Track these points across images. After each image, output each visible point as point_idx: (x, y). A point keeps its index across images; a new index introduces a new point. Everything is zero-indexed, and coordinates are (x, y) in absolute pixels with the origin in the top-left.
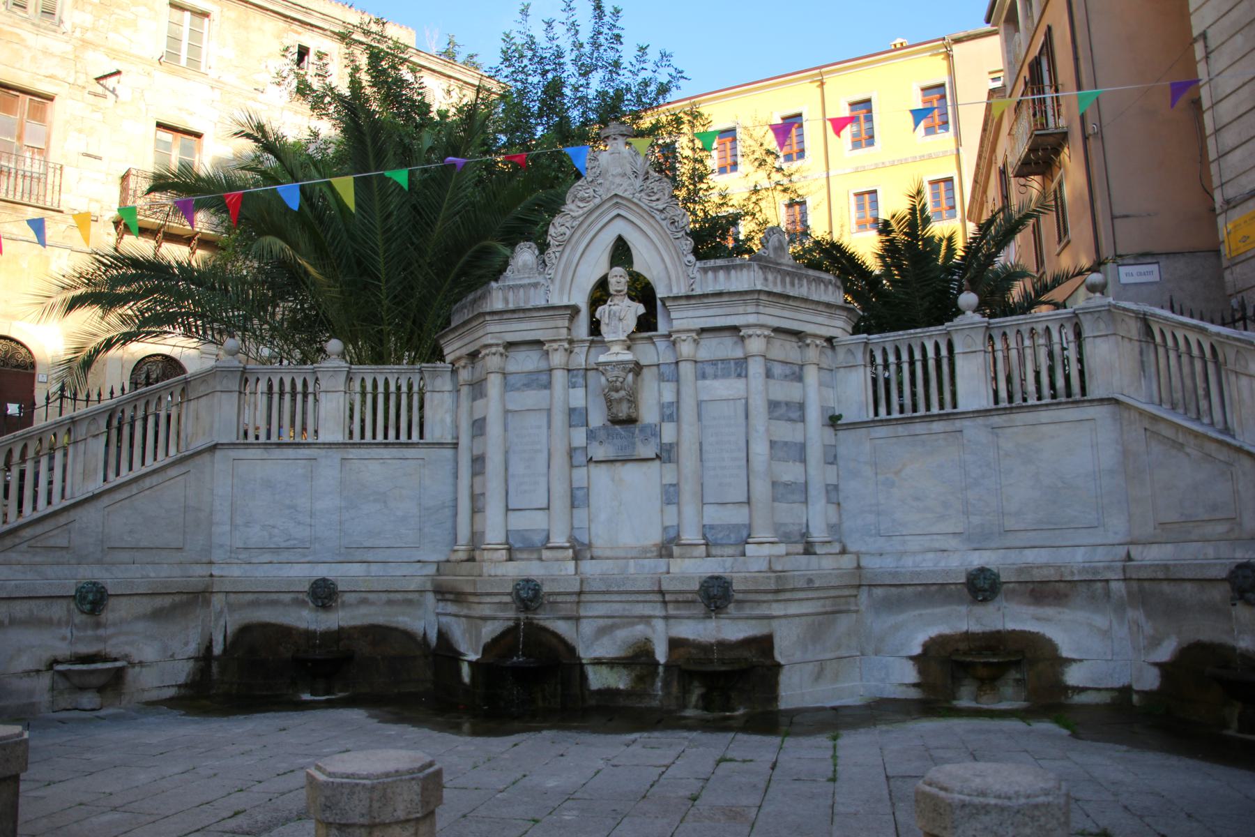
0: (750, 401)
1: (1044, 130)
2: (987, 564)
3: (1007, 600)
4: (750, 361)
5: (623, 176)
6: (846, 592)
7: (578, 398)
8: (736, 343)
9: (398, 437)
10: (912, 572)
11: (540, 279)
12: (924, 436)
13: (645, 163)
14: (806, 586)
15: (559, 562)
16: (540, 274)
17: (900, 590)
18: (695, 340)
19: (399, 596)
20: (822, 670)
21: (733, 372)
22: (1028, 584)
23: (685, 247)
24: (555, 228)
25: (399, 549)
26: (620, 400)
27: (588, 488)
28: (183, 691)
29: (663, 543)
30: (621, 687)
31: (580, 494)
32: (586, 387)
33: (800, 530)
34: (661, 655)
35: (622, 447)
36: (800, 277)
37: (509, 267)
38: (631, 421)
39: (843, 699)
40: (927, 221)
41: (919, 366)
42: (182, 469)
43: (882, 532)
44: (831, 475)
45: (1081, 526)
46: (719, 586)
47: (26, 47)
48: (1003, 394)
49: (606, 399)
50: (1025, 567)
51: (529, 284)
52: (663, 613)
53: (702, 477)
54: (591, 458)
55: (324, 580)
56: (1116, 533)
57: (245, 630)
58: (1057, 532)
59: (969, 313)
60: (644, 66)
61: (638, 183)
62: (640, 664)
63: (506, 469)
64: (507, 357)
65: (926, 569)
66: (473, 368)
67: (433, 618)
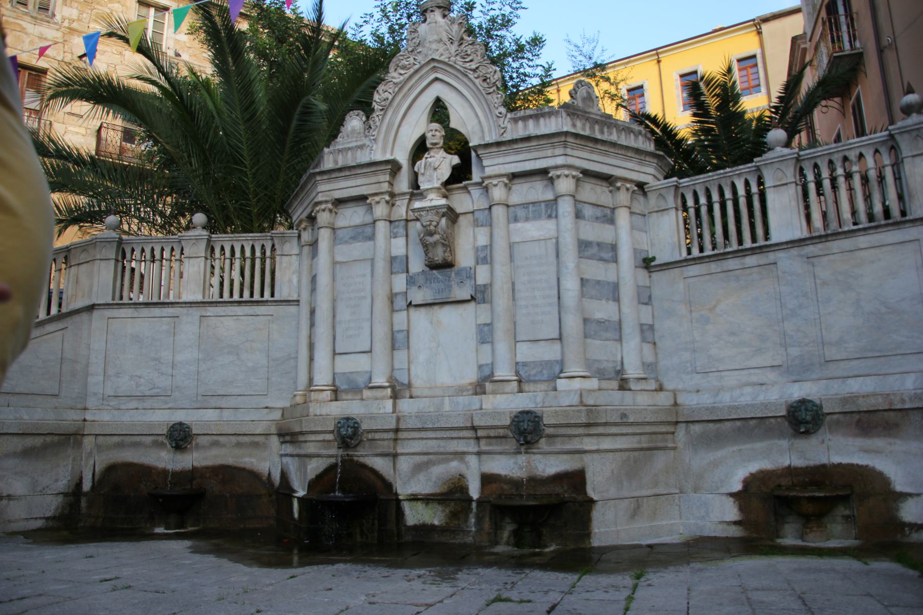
0: (561, 240)
1: (842, 51)
2: (808, 396)
3: (831, 432)
4: (560, 201)
5: (439, 42)
6: (663, 429)
7: (399, 247)
8: (546, 186)
9: (252, 295)
10: (729, 407)
11: (366, 141)
12: (737, 272)
13: (460, 31)
14: (620, 421)
15: (378, 401)
16: (366, 136)
17: (718, 425)
18: (506, 185)
19: (246, 439)
20: (638, 507)
21: (543, 214)
22: (854, 415)
23: (496, 100)
24: (380, 95)
25: (249, 397)
26: (435, 244)
27: (408, 332)
28: (51, 523)
29: (478, 382)
30: (436, 523)
31: (400, 337)
32: (407, 236)
33: (615, 367)
34: (474, 492)
35: (439, 290)
37: (341, 134)
38: (447, 265)
39: (661, 537)
40: (736, 98)
41: (730, 206)
42: (60, 325)
43: (698, 368)
45: (908, 352)
46: (529, 421)
47: (26, 33)
49: (422, 245)
50: (850, 397)
51: (356, 146)
52: (476, 450)
53: (514, 316)
54: (411, 303)
55: (181, 424)
57: (111, 469)
58: (883, 359)
60: (493, 6)
62: (453, 500)
63: (334, 316)
64: (336, 213)
65: (744, 403)
66: (313, 230)
67: (277, 459)
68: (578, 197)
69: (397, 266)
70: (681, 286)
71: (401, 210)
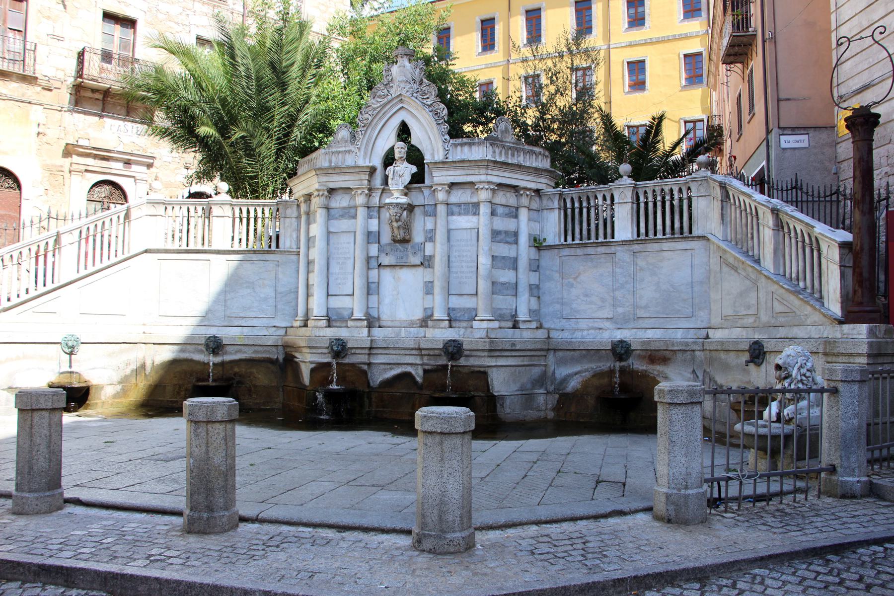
7: (374, 225)
17: (572, 353)
27: (378, 283)
31: (373, 286)
32: (379, 218)
36: (518, 150)
38: (405, 241)
44: (534, 278)
48: (643, 230)
53: (449, 277)
56: (702, 321)
59: (625, 177)
61: (416, 86)
63: (328, 269)
68: (494, 201)
69: (372, 239)
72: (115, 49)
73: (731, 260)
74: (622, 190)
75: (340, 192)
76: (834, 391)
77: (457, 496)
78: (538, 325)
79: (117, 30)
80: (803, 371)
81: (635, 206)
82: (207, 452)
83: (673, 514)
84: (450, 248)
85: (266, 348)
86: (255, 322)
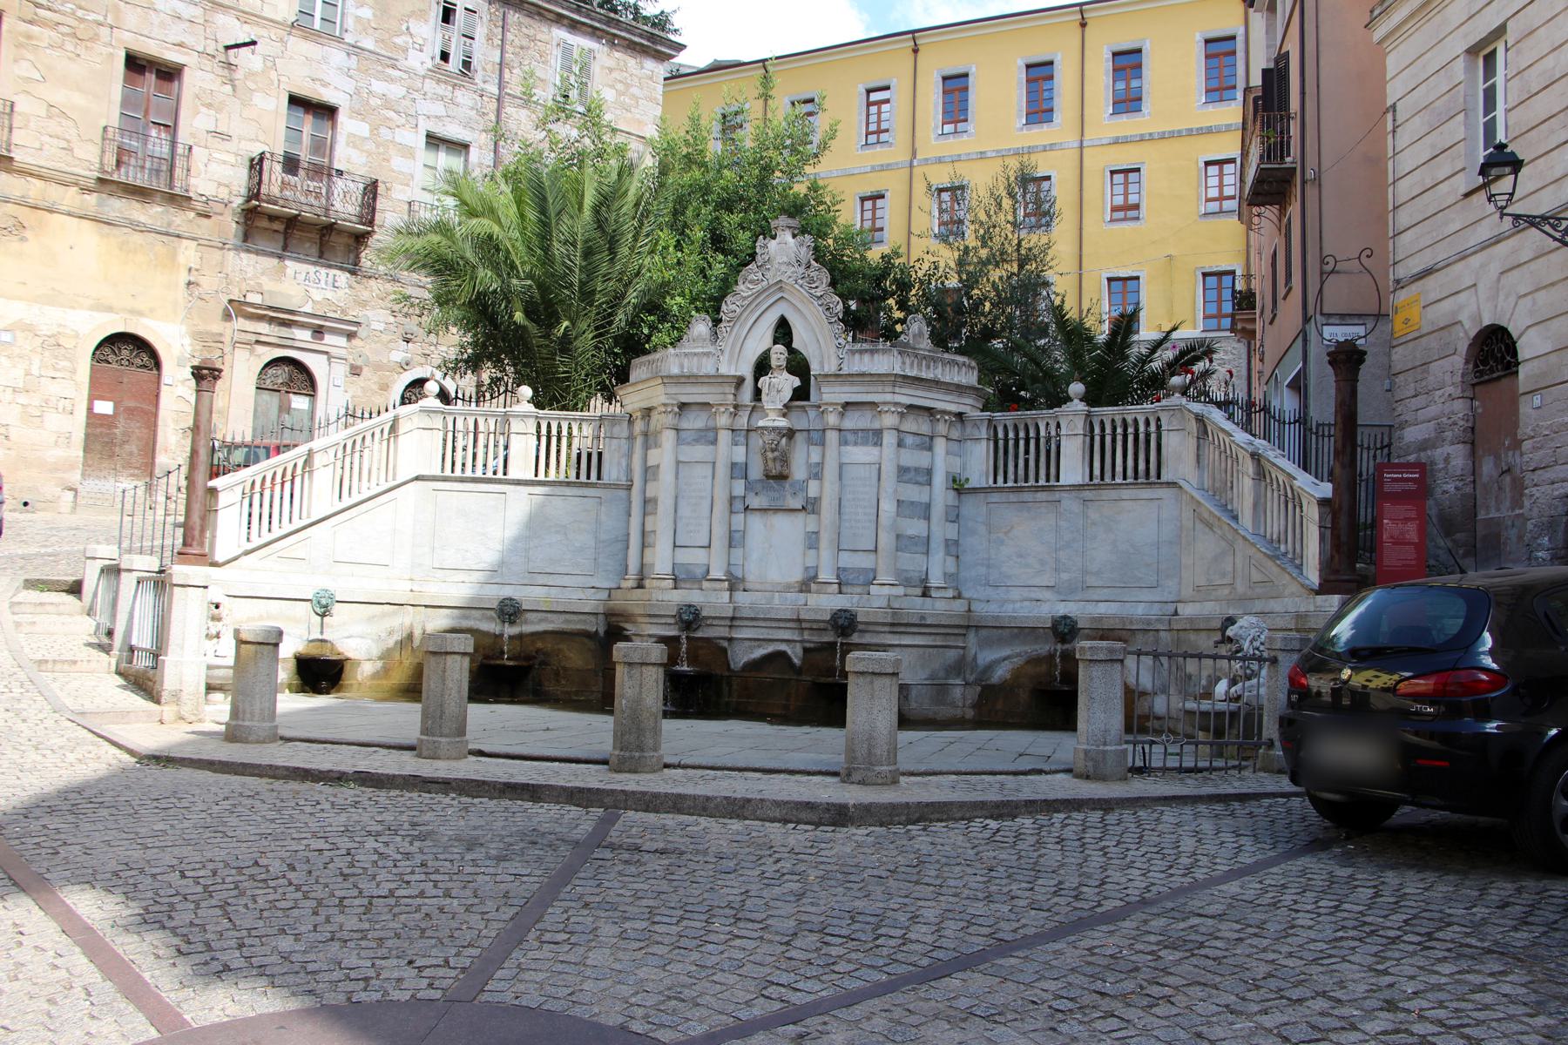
7: (739, 454)
31: (737, 536)
36: (934, 360)
38: (782, 477)
44: (951, 531)
48: (1097, 472)
59: (1076, 401)
61: (801, 270)
68: (903, 428)
70: (984, 509)
71: (742, 421)
72: (305, 155)
73: (1206, 515)
74: (1071, 417)
75: (694, 407)
76: (1274, 661)
77: (885, 732)
78: (956, 594)
79: (308, 124)
80: (1256, 644)
81: (1088, 439)
82: (641, 692)
83: (1091, 770)
84: (842, 487)
85: (581, 617)
86: (566, 581)
